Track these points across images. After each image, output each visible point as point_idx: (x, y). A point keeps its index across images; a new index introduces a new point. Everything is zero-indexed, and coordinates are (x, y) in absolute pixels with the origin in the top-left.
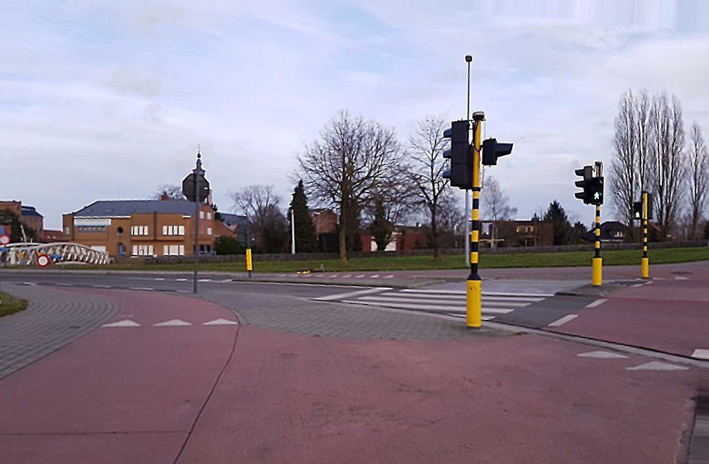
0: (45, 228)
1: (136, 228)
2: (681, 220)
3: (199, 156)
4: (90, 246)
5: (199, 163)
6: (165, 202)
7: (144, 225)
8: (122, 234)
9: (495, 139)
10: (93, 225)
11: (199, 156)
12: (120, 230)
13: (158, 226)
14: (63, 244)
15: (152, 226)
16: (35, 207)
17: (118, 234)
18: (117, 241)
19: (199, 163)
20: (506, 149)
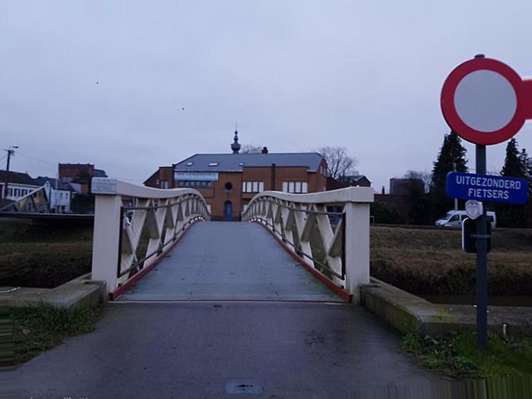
0: (487, 146)
1: (249, 184)
2: (31, 330)
3: (236, 133)
4: (208, 204)
5: (236, 139)
6: (264, 155)
7: (259, 181)
8: (231, 191)
9: (93, 166)
10: (197, 179)
11: (236, 133)
12: (229, 186)
13: (276, 180)
14: (24, 213)
15: (270, 181)
16: (105, 170)
17: (226, 191)
18: (225, 199)
19: (236, 139)
20: (265, 148)
